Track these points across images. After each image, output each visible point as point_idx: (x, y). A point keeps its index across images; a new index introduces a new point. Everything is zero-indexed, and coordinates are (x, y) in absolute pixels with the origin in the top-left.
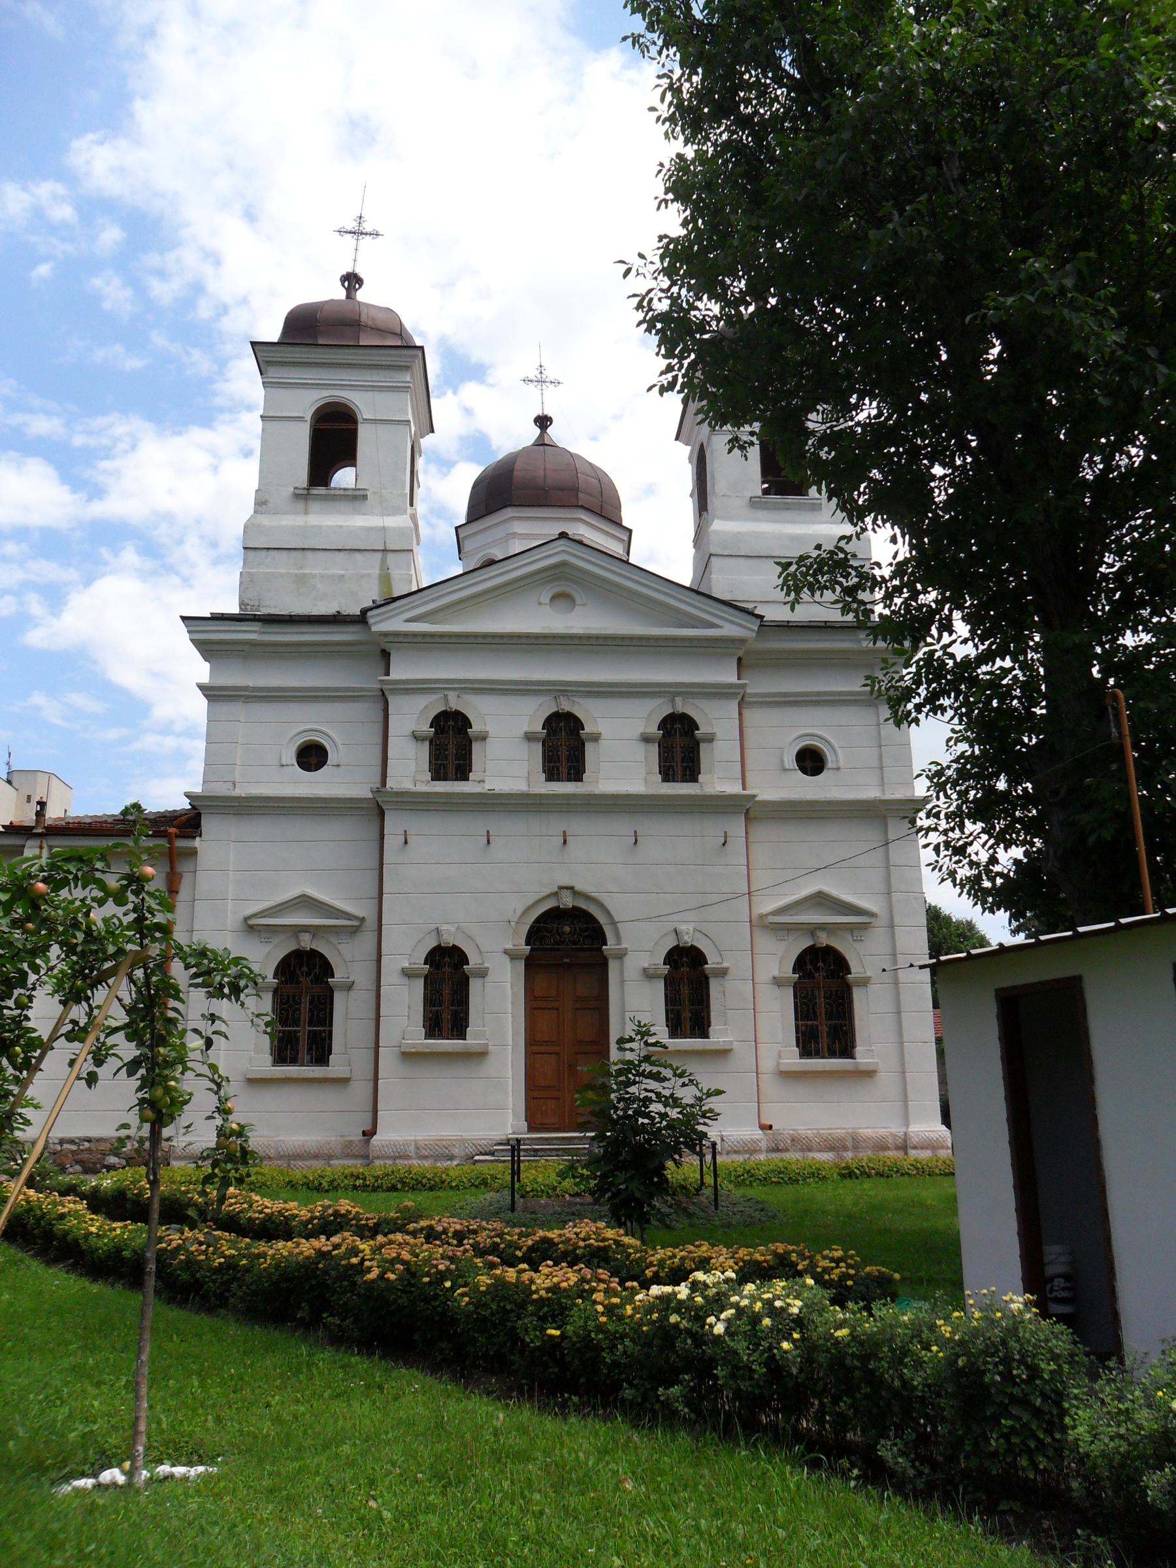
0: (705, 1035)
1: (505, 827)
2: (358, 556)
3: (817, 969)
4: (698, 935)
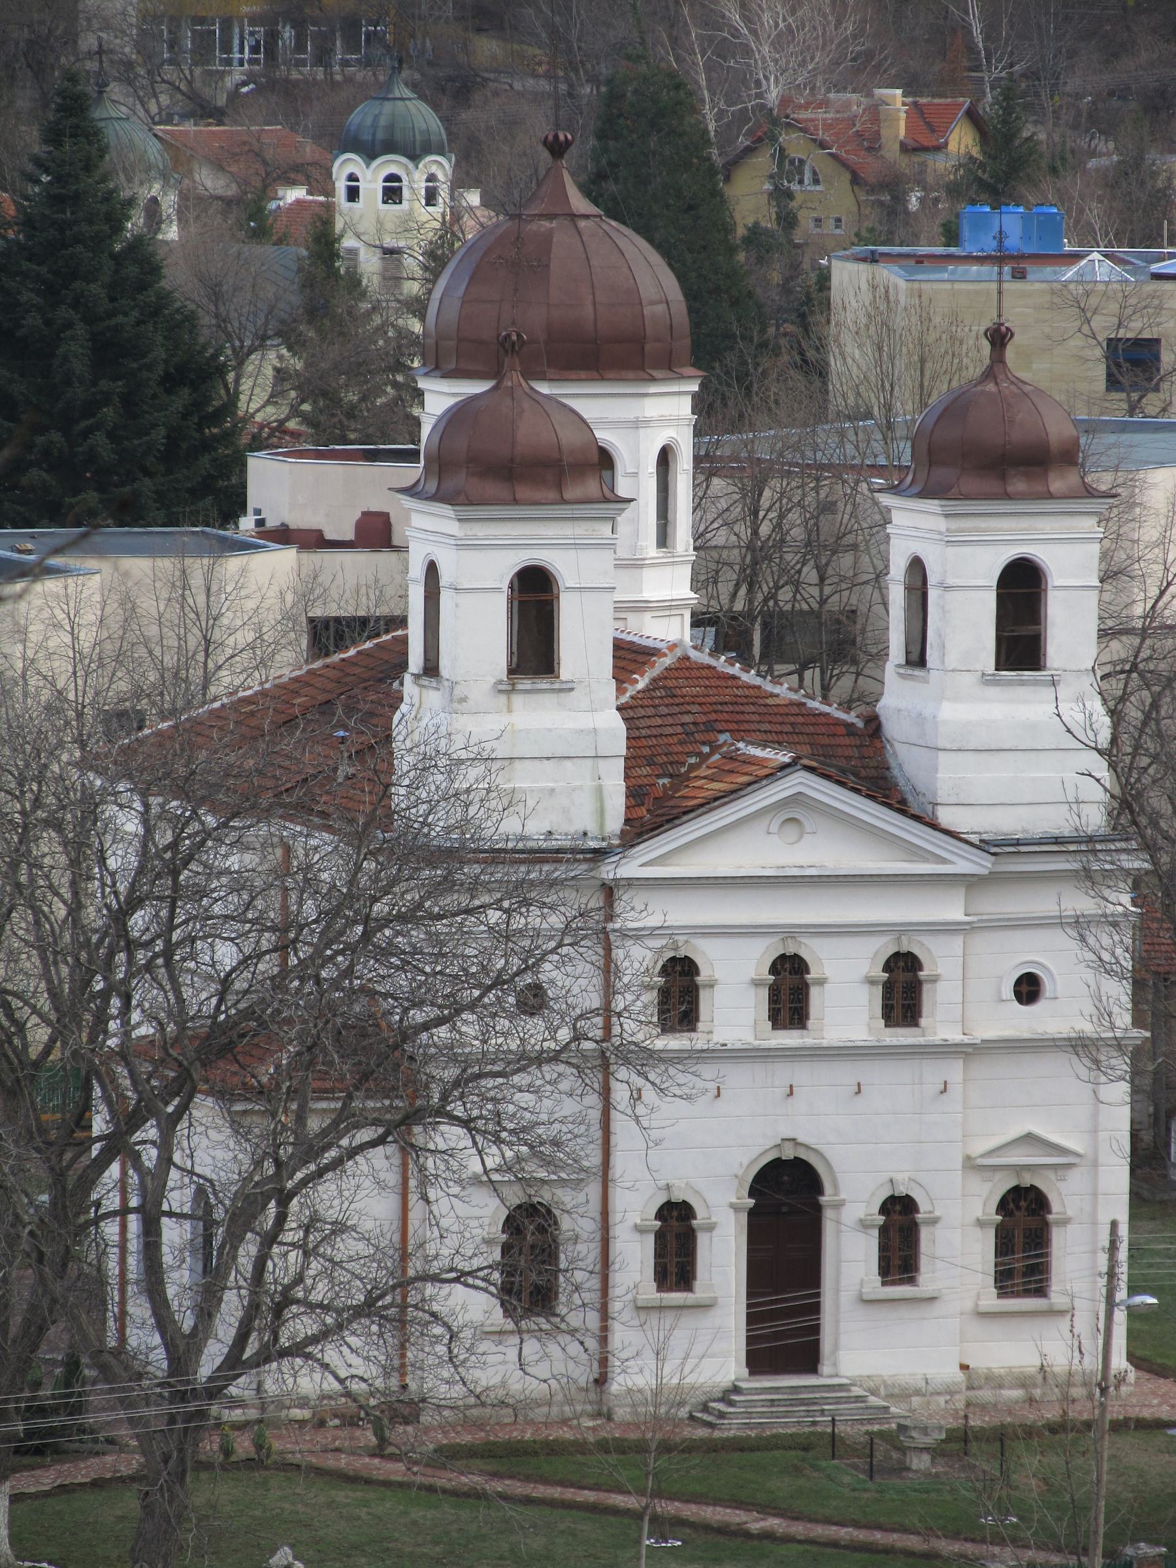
0: (912, 1281)
1: (737, 1077)
2: (568, 764)
3: (1019, 1208)
4: (913, 1184)
